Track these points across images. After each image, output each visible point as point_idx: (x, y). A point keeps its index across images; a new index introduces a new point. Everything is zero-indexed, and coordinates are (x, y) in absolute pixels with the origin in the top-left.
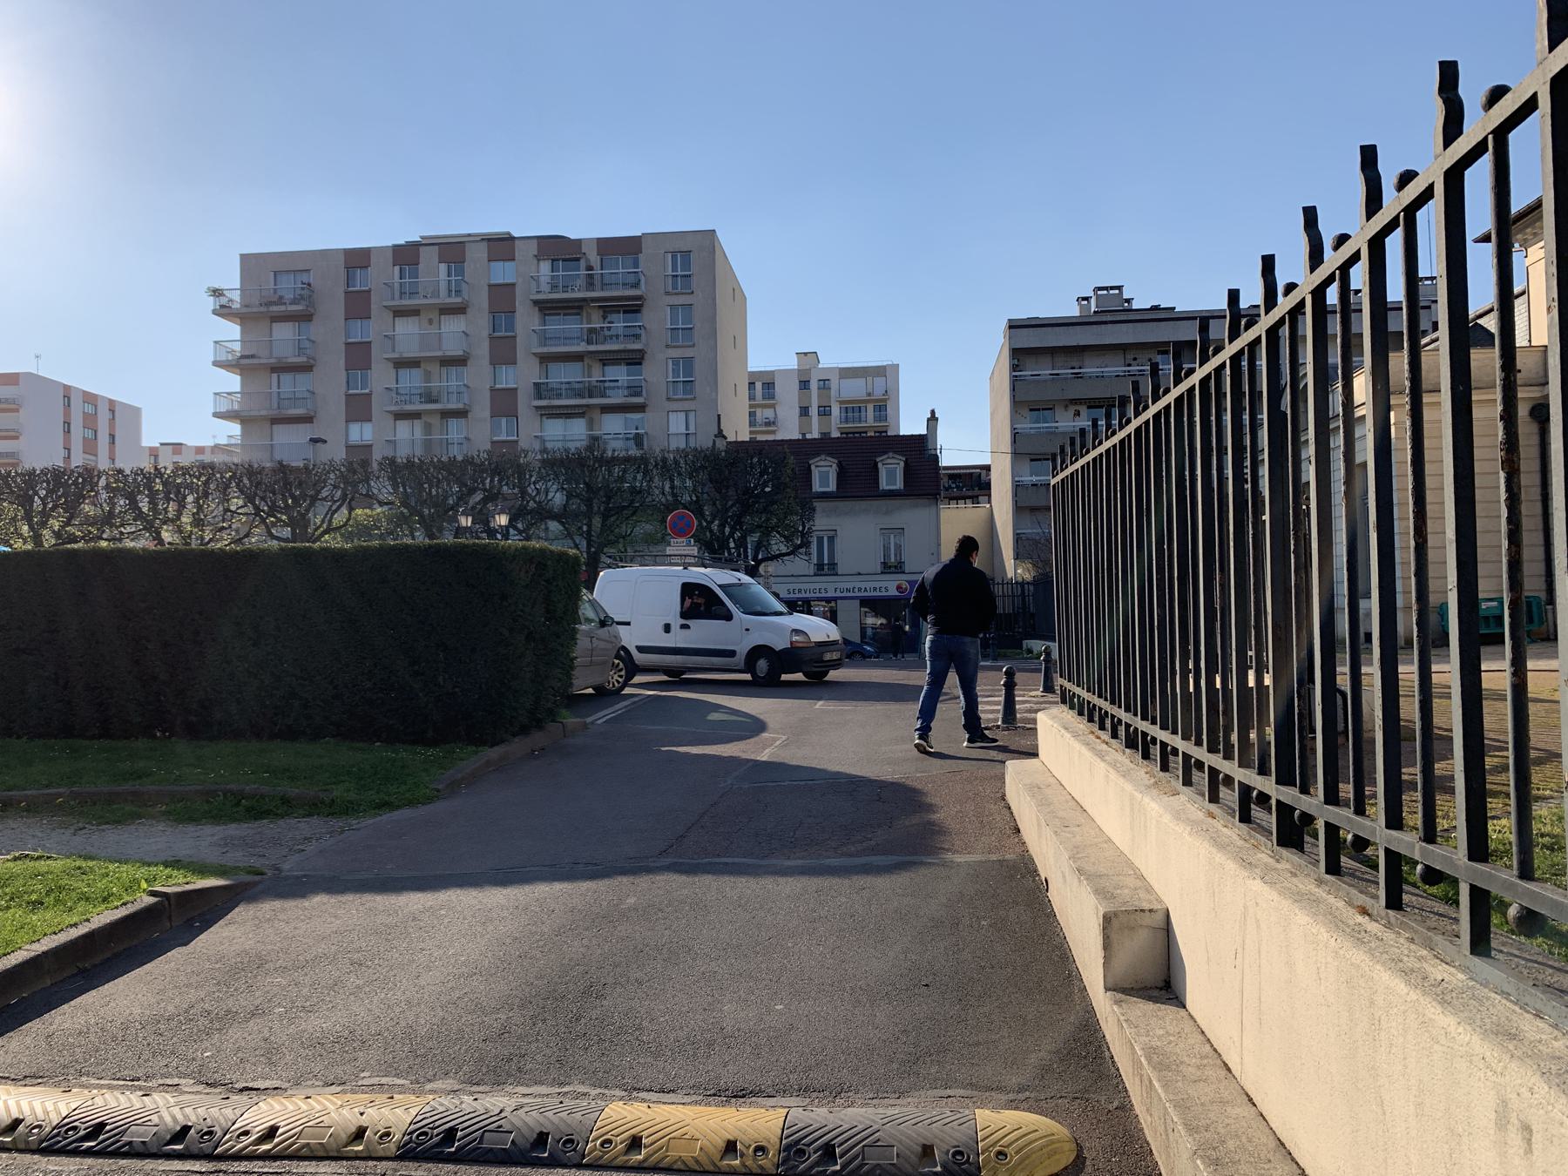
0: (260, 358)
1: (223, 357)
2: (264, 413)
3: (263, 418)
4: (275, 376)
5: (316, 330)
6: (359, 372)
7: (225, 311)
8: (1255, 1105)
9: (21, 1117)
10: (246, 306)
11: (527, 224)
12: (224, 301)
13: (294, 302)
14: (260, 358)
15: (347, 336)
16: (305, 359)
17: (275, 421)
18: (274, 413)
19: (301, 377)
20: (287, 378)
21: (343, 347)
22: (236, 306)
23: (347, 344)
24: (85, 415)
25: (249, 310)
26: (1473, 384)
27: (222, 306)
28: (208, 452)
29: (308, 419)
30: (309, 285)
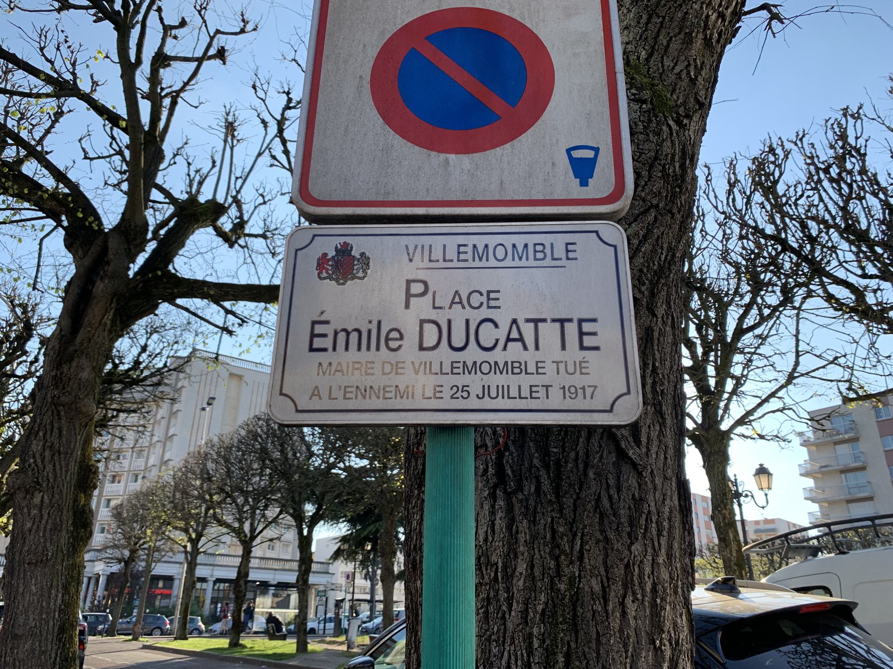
0: (832, 466)
1: (803, 472)
2: (842, 497)
3: (841, 501)
4: (843, 475)
5: (863, 445)
6: (189, 617)
7: (807, 443)
8: (82, 148)
9: (267, 615)
10: (818, 439)
11: (425, 541)
12: (805, 438)
13: (846, 432)
14: (832, 466)
15: (884, 446)
16: (861, 464)
17: (849, 502)
18: (849, 497)
19: (860, 474)
20: (850, 475)
21: (883, 454)
22: (812, 440)
23: (885, 451)
24: (704, 508)
25: (819, 441)
26: (236, 569)
27: (805, 441)
28: (762, 523)
29: (870, 499)
30: (853, 421)
